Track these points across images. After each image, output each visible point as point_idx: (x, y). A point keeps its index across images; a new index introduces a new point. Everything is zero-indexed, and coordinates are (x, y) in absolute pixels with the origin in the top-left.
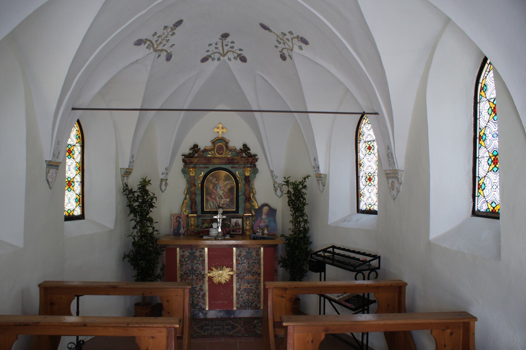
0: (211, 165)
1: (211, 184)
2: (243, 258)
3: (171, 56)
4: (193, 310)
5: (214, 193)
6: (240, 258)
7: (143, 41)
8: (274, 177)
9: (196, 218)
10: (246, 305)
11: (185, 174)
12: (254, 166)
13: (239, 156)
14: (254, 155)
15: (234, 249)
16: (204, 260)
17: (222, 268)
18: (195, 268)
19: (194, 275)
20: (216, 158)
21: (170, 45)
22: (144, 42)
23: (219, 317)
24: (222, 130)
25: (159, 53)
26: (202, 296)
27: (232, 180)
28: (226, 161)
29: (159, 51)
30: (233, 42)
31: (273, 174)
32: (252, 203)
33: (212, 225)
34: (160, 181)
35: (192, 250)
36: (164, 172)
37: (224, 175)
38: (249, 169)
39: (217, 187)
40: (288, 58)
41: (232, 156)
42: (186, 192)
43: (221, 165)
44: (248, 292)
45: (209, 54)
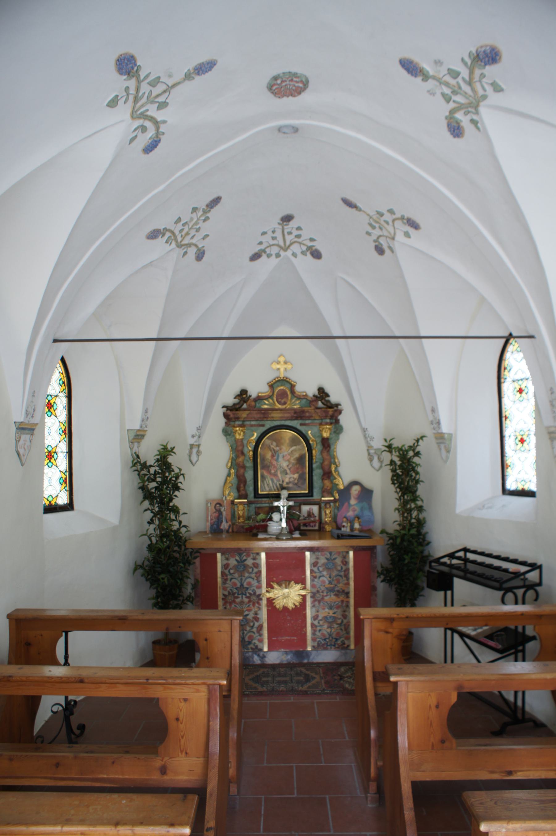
3: (204, 253)
5: (274, 465)
7: (161, 232)
8: (369, 439)
10: (328, 642)
15: (308, 554)
18: (245, 585)
19: (244, 596)
21: (202, 237)
22: (161, 233)
23: (285, 662)
24: (285, 366)
25: (185, 250)
26: (257, 628)
28: (292, 414)
29: (186, 246)
30: (299, 228)
36: (195, 434)
40: (387, 251)
41: (302, 407)
45: (262, 247)
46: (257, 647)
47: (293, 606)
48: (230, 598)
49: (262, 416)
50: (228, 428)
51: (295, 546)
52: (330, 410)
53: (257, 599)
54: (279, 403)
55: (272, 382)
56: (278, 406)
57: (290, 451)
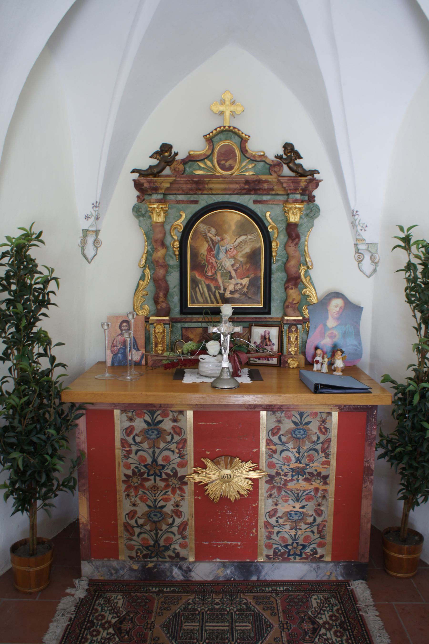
0: (205, 196)
1: (205, 243)
2: (284, 439)
4: (158, 561)
5: (212, 263)
6: (277, 437)
8: (359, 228)
9: (168, 326)
10: (290, 550)
11: (141, 218)
12: (308, 199)
13: (272, 173)
14: (310, 171)
15: (263, 414)
16: (185, 441)
17: (231, 463)
18: (160, 461)
19: (158, 478)
20: (217, 177)
23: (221, 579)
24: (232, 108)
26: (179, 527)
27: (256, 233)
28: (242, 185)
31: (355, 220)
32: (304, 290)
33: (205, 345)
34: (82, 235)
35: (153, 417)
36: (90, 214)
37: (235, 221)
38: (297, 206)
39: (219, 249)
41: (256, 174)
42: (144, 261)
43: (230, 194)
44: (295, 521)
46: (178, 554)
47: (238, 497)
48: (135, 480)
49: (194, 186)
50: (141, 204)
51: (243, 404)
52: (303, 179)
53: (179, 483)
54: (223, 168)
55: (211, 134)
56: (220, 171)
57: (237, 243)
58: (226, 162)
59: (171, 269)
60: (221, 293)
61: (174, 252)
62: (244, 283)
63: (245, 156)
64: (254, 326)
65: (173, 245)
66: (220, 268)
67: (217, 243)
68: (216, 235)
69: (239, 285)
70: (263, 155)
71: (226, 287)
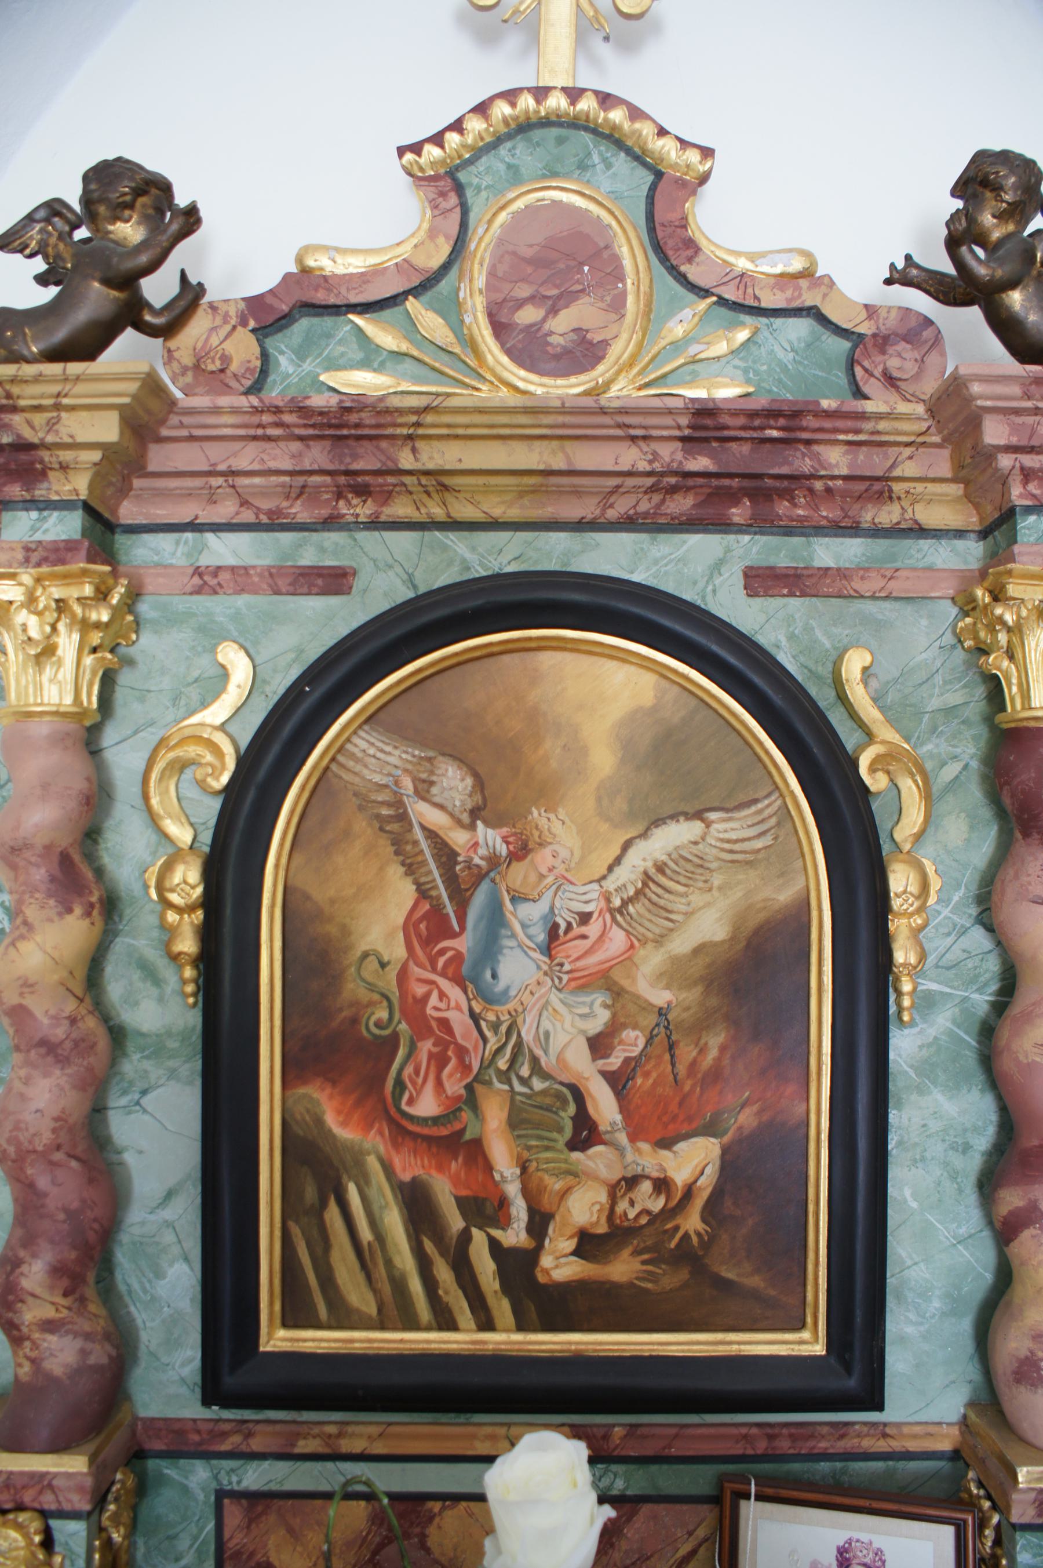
0: (403, 541)
1: (395, 871)
5: (445, 1024)
27: (769, 805)
37: (616, 710)
39: (496, 919)
43: (580, 526)
57: (627, 875)
58: (554, 311)
59: (147, 1065)
60: (514, 1251)
61: (170, 933)
62: (680, 1177)
63: (682, 279)
64: (759, 1498)
65: (160, 889)
66: (502, 1064)
67: (480, 876)
68: (475, 813)
69: (646, 1186)
70: (807, 274)
71: (546, 1203)
